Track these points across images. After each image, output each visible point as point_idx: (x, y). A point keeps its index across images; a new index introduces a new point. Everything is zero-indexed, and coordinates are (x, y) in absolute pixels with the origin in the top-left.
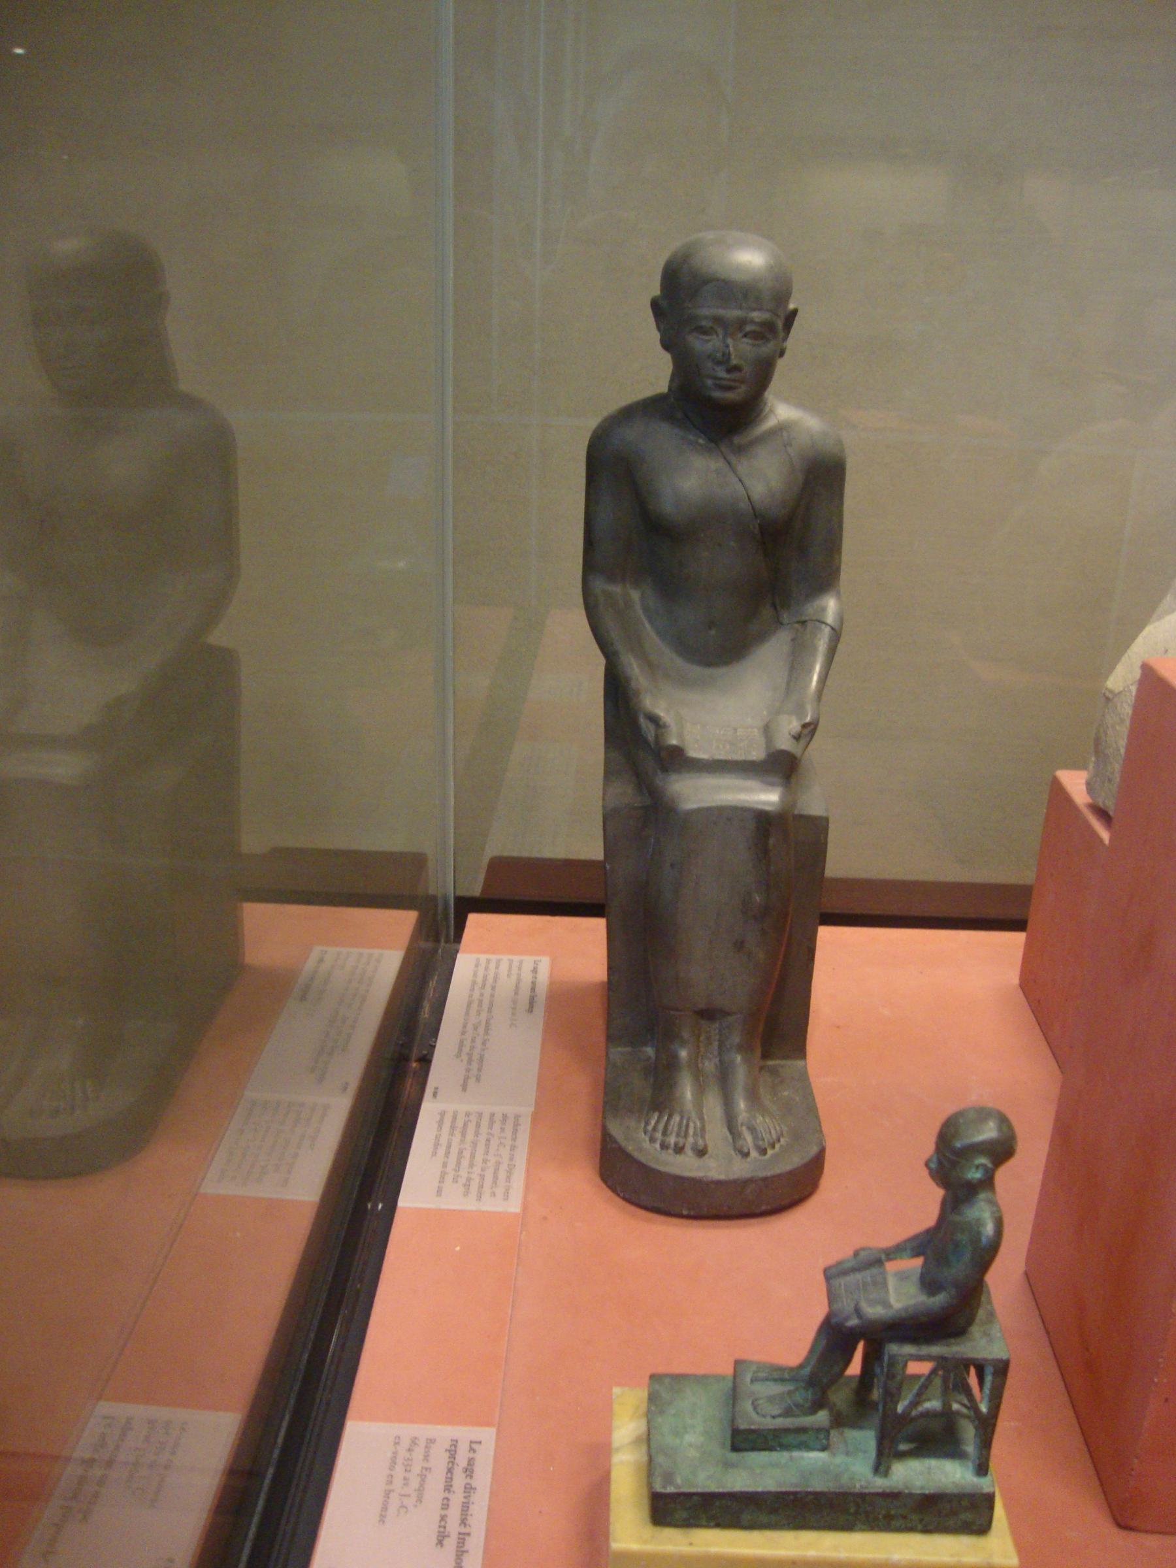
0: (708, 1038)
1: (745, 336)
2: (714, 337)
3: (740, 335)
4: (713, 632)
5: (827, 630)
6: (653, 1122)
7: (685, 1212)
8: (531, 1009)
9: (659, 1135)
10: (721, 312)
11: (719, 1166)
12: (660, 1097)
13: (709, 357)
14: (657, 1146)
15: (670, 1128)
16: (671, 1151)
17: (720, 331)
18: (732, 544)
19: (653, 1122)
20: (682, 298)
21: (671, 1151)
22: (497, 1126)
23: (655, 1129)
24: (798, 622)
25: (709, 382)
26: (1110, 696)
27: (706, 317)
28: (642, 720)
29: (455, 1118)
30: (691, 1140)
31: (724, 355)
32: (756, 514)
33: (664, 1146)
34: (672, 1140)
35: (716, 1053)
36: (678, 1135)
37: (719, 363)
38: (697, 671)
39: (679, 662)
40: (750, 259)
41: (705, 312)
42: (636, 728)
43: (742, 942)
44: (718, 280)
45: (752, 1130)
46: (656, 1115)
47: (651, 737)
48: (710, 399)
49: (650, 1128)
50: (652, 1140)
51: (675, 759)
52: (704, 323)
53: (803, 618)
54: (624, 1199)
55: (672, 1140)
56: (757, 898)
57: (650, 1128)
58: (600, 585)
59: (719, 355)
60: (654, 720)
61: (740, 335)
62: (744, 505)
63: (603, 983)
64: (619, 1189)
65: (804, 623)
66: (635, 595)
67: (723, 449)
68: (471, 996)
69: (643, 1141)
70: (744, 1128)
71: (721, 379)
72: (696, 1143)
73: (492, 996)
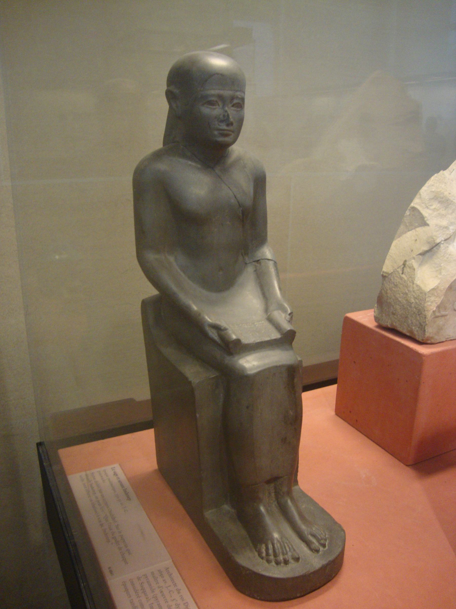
0: (270, 494)
1: (233, 106)
2: (217, 107)
3: (230, 105)
4: (221, 273)
5: (271, 264)
6: (264, 550)
7: (298, 595)
8: (129, 499)
9: (272, 557)
10: (221, 92)
11: (316, 562)
12: (256, 534)
13: (216, 118)
14: (273, 563)
15: (277, 551)
16: (282, 564)
17: (220, 103)
18: (228, 223)
19: (264, 550)
20: (186, 84)
21: (282, 564)
22: (160, 580)
23: (267, 554)
24: (254, 262)
25: (216, 133)
26: (387, 275)
27: (213, 95)
28: (207, 329)
29: (133, 584)
30: (290, 554)
31: (224, 116)
32: (240, 205)
33: (278, 563)
34: (281, 558)
35: (274, 499)
36: (283, 554)
37: (222, 121)
38: (214, 296)
39: (205, 292)
40: (218, 62)
41: (213, 92)
42: (205, 335)
43: (286, 438)
44: (218, 74)
45: (314, 536)
46: (264, 546)
47: (216, 338)
48: (217, 142)
49: (264, 555)
50: (269, 561)
51: (235, 347)
52: (213, 99)
53: (258, 259)
54: (261, 600)
55: (281, 558)
56: (291, 413)
57: (264, 555)
58: (151, 256)
59: (221, 117)
60: (217, 328)
61: (230, 105)
62: (233, 201)
63: (156, 470)
64: (256, 595)
65: (258, 261)
66: (171, 259)
67: (217, 171)
68: (91, 501)
69: (248, 560)
70: (309, 536)
71: (224, 130)
72: (292, 556)
73: (103, 496)
